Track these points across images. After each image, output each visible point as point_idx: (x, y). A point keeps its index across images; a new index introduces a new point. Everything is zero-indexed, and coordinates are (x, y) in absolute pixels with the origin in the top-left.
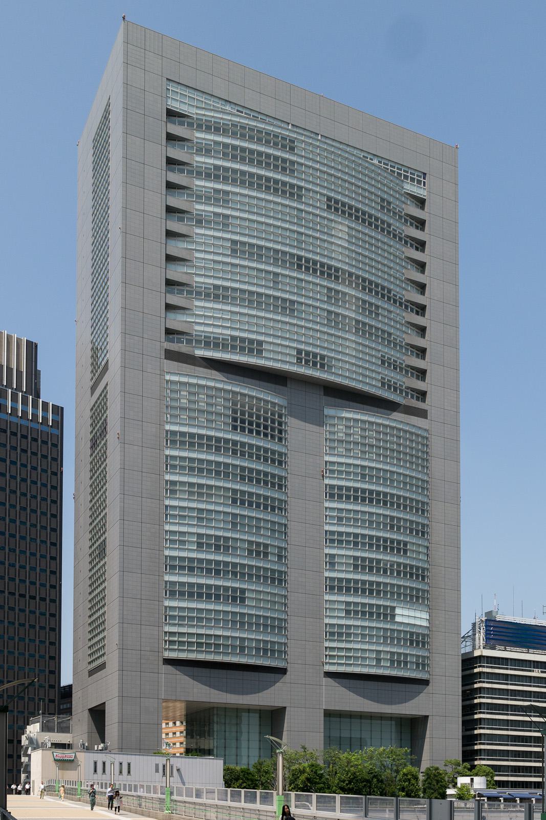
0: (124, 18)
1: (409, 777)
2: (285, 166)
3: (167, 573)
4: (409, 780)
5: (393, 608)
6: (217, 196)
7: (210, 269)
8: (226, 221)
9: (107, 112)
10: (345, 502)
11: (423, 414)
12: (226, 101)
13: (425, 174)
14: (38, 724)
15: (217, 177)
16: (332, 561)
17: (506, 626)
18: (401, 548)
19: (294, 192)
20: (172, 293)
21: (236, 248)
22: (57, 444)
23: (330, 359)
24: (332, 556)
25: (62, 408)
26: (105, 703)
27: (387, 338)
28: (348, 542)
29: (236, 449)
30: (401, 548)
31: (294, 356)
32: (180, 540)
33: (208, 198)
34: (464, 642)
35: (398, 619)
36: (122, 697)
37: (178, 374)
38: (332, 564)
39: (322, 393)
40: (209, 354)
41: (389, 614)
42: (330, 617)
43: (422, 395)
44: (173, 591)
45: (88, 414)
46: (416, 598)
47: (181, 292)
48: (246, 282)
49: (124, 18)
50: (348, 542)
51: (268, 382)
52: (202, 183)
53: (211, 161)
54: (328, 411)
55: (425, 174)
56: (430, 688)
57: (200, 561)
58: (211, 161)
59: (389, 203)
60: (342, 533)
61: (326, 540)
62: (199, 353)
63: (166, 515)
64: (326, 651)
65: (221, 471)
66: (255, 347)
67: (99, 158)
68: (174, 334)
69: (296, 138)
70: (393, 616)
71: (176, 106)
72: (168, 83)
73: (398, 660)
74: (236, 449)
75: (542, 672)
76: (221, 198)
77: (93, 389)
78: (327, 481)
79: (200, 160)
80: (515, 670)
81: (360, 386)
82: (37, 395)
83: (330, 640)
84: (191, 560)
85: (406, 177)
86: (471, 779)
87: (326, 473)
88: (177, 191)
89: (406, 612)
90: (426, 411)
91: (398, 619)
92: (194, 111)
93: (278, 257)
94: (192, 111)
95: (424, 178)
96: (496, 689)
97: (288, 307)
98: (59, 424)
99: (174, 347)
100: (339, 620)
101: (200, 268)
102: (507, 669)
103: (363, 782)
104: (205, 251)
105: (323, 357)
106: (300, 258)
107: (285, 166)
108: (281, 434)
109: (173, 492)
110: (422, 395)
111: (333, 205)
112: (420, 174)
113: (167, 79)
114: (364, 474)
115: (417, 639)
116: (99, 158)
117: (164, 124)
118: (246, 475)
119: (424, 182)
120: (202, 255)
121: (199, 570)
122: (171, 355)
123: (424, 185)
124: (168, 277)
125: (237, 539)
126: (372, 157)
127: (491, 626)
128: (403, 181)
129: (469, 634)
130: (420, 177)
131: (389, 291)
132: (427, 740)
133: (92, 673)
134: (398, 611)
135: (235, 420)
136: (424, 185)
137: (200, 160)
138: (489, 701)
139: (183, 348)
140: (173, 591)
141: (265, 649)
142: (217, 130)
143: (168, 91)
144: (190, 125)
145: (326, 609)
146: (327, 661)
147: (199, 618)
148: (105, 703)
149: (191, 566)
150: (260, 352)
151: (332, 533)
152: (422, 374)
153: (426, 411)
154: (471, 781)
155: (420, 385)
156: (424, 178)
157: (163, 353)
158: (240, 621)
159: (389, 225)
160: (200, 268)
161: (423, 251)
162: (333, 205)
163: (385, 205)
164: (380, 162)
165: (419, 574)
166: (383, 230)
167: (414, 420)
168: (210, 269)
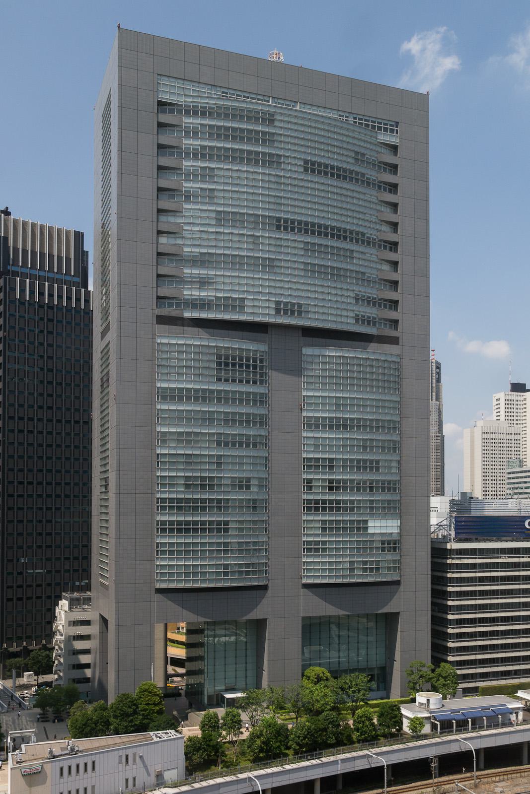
0: (119, 27)
1: (363, 719)
2: (264, 138)
3: (159, 424)
4: (363, 722)
5: (366, 522)
6: (203, 173)
7: (196, 239)
8: (211, 195)
10: (314, 472)
11: (395, 341)
12: (212, 85)
13: (397, 123)
15: (203, 156)
16: (309, 483)
17: (474, 520)
18: (373, 466)
19: (274, 161)
20: (164, 155)
21: (221, 218)
23: (307, 306)
24: (309, 481)
27: (362, 278)
28: (324, 467)
29: (221, 397)
30: (373, 466)
32: (169, 483)
33: (195, 176)
35: (370, 531)
37: (167, 338)
38: (310, 488)
39: (301, 335)
40: (196, 315)
41: (362, 527)
42: (308, 535)
43: (395, 323)
44: (166, 528)
46: (390, 509)
47: (172, 154)
48: (230, 248)
49: (119, 27)
50: (324, 467)
51: (250, 331)
52: (190, 163)
53: (198, 143)
54: (307, 351)
55: (397, 123)
56: (401, 588)
57: (188, 500)
58: (198, 143)
59: (363, 155)
60: (319, 459)
61: (304, 466)
62: (187, 315)
63: (158, 462)
64: (304, 565)
65: (207, 419)
66: (238, 305)
68: (166, 105)
69: (275, 112)
70: (366, 529)
71: (165, 97)
72: (159, 77)
73: (369, 568)
74: (221, 397)
75: (509, 557)
76: (207, 175)
78: (304, 414)
79: (189, 143)
80: (483, 558)
83: (308, 556)
84: (180, 500)
85: (380, 128)
87: (304, 405)
88: (167, 128)
89: (378, 524)
90: (398, 338)
91: (370, 531)
92: (181, 99)
93: (258, 221)
94: (181, 100)
95: (397, 127)
96: (464, 578)
97: (267, 265)
99: (165, 311)
100: (313, 535)
101: (189, 238)
102: (475, 558)
103: (319, 731)
104: (192, 224)
105: (300, 305)
106: (279, 220)
107: (264, 138)
108: (262, 377)
109: (164, 441)
110: (395, 323)
111: (311, 167)
112: (393, 123)
113: (158, 74)
114: (339, 404)
115: (391, 544)
117: (155, 115)
118: (229, 420)
119: (397, 130)
120: (190, 228)
121: (187, 508)
122: (162, 320)
123: (397, 133)
124: (159, 164)
125: (244, 214)
126: (347, 115)
127: (462, 522)
128: (376, 132)
130: (393, 126)
131: (363, 234)
132: (399, 634)
134: (370, 524)
135: (219, 364)
136: (397, 133)
137: (189, 143)
138: (458, 589)
139: (173, 311)
140: (166, 528)
141: (248, 569)
142: (203, 114)
143: (159, 85)
144: (180, 112)
145: (304, 528)
146: (305, 574)
147: (187, 551)
149: (178, 505)
150: (242, 307)
151: (310, 459)
152: (394, 304)
153: (398, 338)
155: (393, 315)
156: (397, 127)
157: (155, 319)
158: (224, 548)
159: (363, 175)
160: (189, 238)
161: (396, 193)
162: (311, 167)
163: (359, 157)
164: (355, 118)
165: (390, 486)
166: (357, 180)
167: (387, 348)
168: (196, 239)
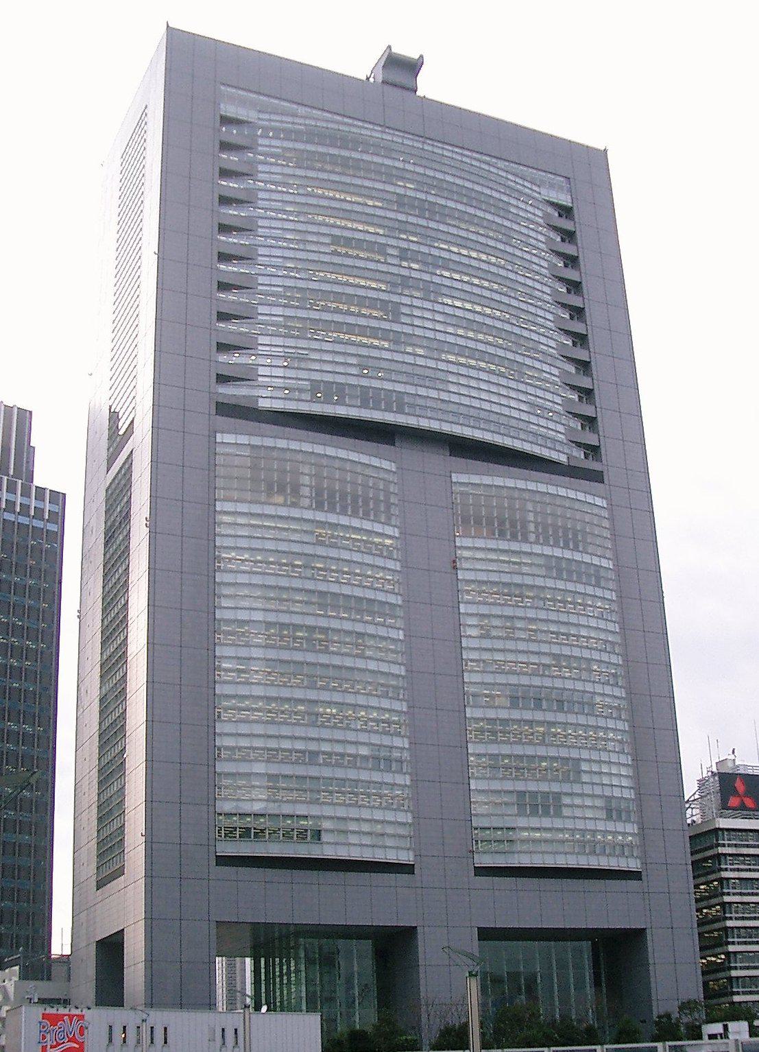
9: (144, 113)
14: (17, 968)
22: (58, 538)
25: (64, 495)
26: (123, 930)
31: (602, 808)
34: (690, 810)
36: (150, 920)
45: (102, 495)
67: (127, 171)
77: (110, 462)
81: (488, 437)
82: (30, 478)
86: (724, 1025)
98: (58, 518)
116: (127, 171)
129: (697, 796)
133: (100, 885)
148: (123, 930)
154: (724, 1031)
